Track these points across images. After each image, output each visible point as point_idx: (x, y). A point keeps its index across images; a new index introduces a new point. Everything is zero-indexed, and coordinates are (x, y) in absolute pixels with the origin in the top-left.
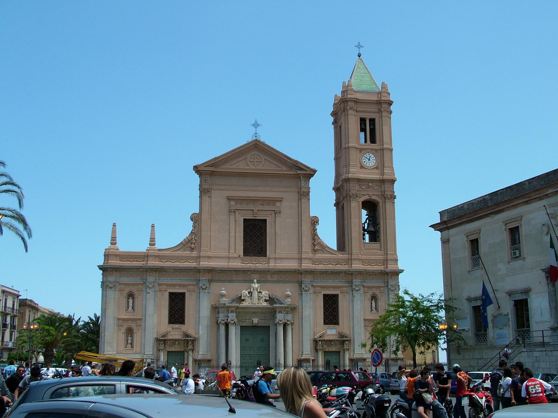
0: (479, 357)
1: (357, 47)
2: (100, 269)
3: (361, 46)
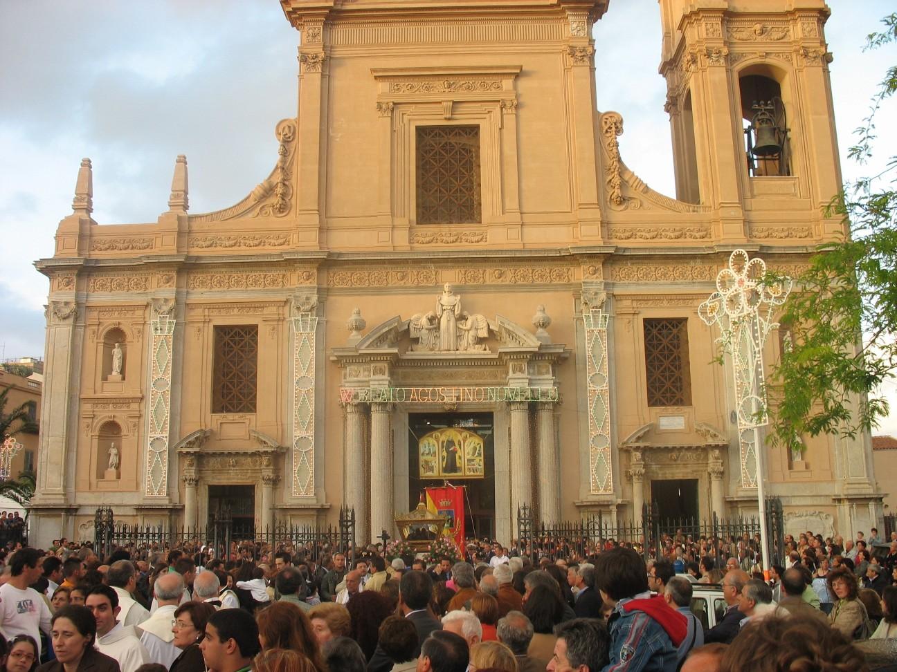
2: (42, 271)
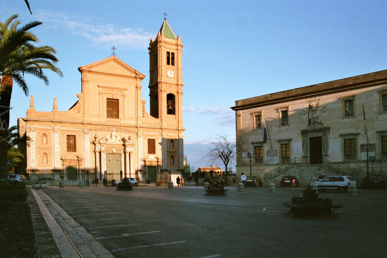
0: (257, 169)
1: (164, 14)
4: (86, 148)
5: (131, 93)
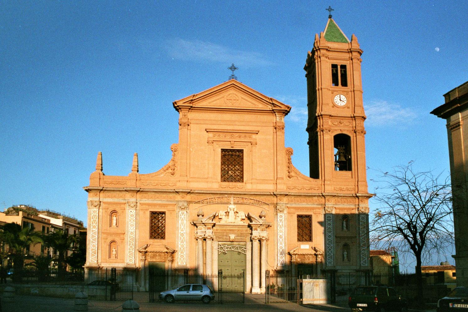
1: (328, 10)
3: (331, 9)
4: (182, 232)
5: (265, 137)
